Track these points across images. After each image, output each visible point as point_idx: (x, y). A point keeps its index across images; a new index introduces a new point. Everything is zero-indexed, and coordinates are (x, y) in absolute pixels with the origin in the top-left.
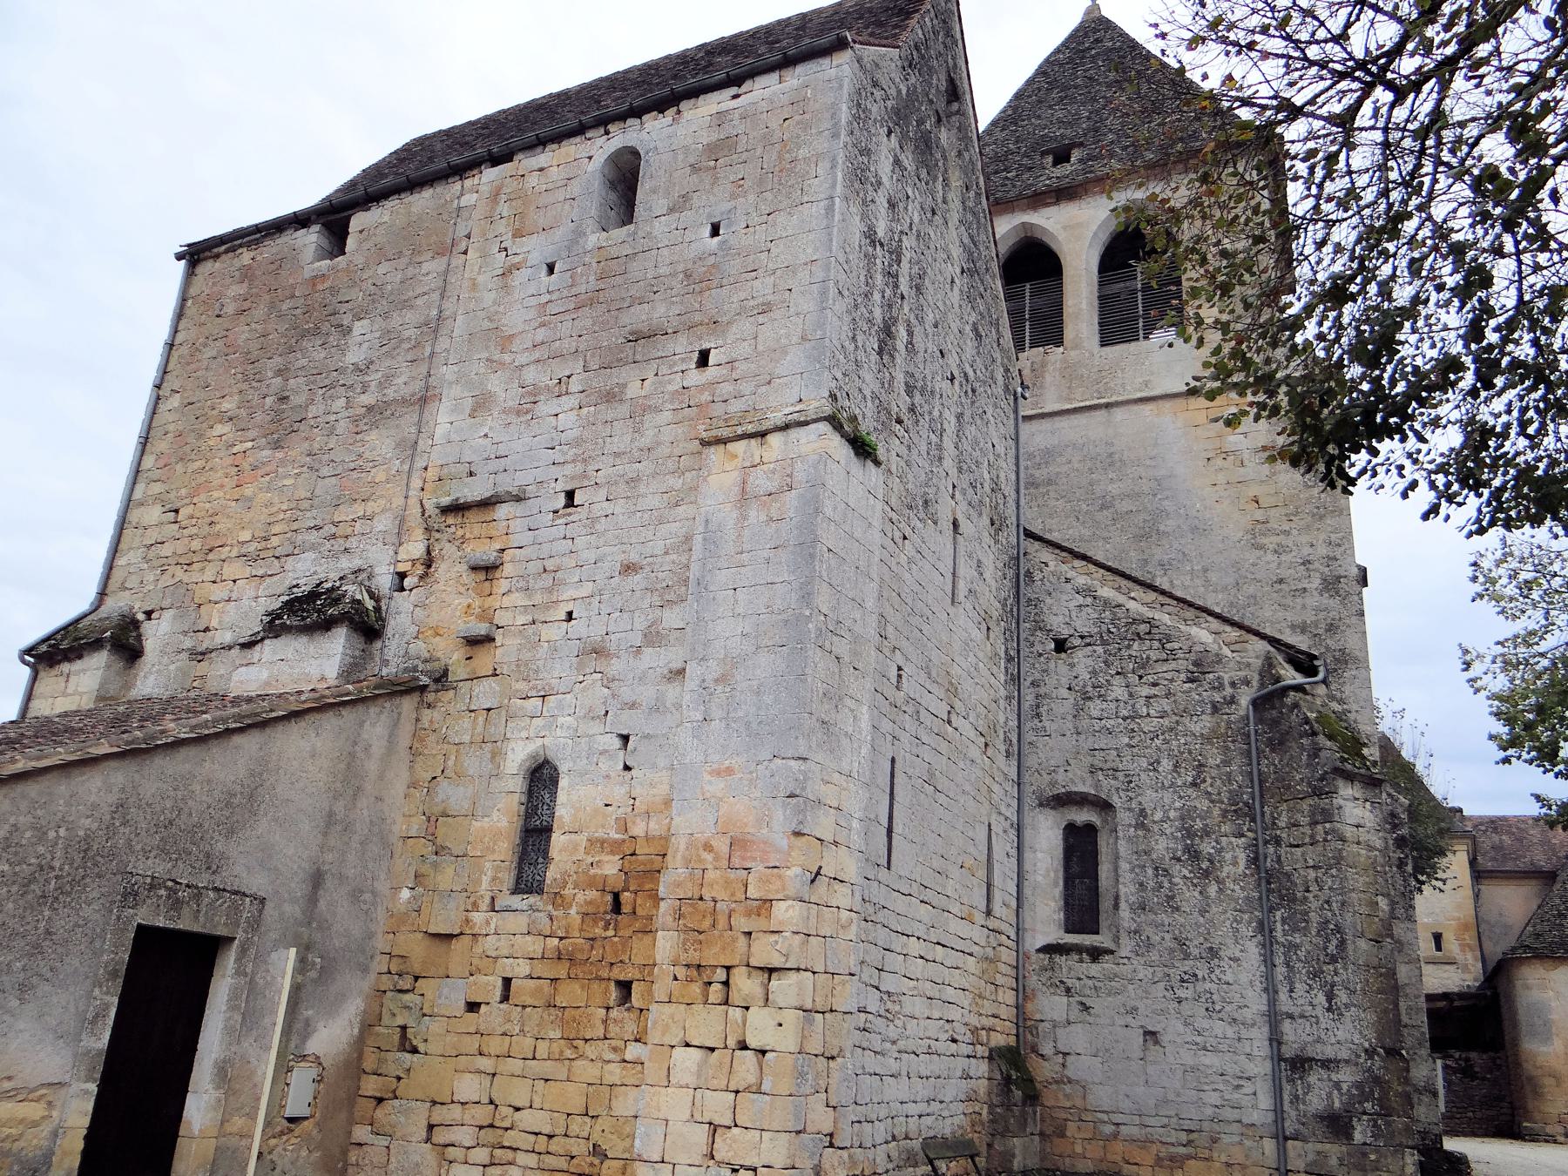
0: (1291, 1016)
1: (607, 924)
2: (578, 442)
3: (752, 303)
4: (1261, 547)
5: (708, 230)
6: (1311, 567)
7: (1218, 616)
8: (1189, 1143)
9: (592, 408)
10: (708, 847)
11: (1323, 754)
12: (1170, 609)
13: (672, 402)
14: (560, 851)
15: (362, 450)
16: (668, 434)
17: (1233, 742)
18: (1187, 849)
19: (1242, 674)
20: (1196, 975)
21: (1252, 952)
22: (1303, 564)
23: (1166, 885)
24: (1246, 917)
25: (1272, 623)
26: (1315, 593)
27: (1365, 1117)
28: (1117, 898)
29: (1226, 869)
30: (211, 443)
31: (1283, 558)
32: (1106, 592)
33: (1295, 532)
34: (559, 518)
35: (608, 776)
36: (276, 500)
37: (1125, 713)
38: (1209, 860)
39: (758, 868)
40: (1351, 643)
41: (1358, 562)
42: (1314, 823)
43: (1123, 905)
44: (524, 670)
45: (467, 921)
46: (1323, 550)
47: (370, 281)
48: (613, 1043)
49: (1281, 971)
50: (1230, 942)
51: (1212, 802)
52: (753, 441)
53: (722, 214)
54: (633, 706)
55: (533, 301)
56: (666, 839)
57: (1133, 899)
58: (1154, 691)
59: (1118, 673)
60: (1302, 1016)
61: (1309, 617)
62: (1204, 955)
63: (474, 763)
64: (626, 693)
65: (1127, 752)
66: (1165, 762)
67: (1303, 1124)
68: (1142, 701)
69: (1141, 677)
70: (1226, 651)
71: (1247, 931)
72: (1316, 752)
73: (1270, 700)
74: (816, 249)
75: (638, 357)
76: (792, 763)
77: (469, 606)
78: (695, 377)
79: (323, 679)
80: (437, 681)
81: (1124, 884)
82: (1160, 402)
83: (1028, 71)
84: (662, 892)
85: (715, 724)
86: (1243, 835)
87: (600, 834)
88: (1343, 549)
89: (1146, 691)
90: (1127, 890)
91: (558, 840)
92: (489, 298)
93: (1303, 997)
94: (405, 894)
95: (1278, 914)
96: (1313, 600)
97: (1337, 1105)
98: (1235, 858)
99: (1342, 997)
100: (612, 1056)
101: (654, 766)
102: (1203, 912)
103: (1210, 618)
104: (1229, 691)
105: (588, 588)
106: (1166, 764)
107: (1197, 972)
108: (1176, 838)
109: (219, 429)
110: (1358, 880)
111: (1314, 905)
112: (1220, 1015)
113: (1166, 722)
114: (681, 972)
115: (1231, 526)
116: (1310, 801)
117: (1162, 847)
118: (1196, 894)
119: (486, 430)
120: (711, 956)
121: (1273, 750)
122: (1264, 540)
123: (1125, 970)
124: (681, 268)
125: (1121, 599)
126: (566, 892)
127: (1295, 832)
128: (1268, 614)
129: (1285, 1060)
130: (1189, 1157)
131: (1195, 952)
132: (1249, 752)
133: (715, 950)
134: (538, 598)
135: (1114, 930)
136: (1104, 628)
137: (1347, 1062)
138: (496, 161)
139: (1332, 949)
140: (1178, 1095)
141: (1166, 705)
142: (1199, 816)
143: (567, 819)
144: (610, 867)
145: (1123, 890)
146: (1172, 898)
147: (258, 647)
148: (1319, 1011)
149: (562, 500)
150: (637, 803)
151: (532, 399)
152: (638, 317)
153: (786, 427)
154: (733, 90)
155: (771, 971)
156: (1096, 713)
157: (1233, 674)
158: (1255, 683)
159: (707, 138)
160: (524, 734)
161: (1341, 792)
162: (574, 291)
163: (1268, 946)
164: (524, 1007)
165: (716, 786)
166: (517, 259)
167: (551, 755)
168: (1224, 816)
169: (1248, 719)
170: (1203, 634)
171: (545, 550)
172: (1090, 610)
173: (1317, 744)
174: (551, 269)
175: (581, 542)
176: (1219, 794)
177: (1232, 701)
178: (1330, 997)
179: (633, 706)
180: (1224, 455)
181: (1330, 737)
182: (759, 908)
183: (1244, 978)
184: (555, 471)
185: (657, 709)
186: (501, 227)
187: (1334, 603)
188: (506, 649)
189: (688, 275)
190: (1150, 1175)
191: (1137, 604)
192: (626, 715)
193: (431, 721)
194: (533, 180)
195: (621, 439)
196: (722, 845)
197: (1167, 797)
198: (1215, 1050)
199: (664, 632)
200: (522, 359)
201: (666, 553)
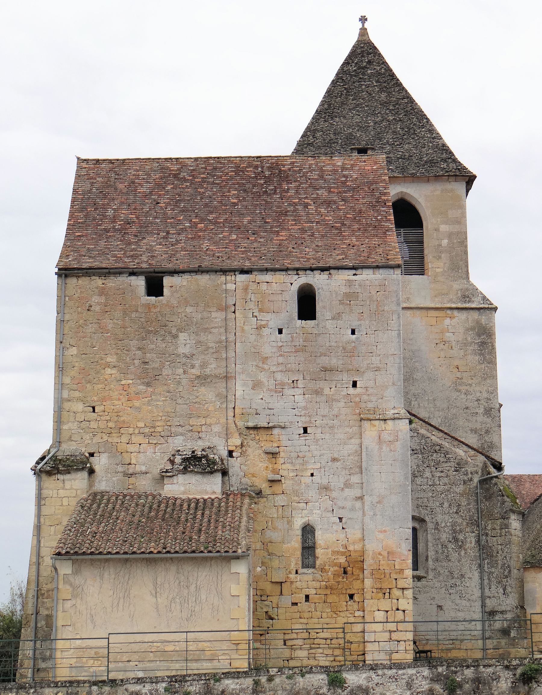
0: (490, 597)
1: (343, 578)
2: (305, 408)
3: (372, 366)
4: (459, 391)
6: (480, 402)
7: (467, 445)
8: (453, 643)
9: (310, 396)
10: (380, 554)
11: (506, 504)
12: (448, 440)
13: (344, 399)
14: (322, 555)
15: (198, 394)
16: (344, 411)
17: (471, 496)
18: (454, 538)
19: (475, 469)
20: (456, 585)
21: (476, 575)
22: (477, 401)
23: (446, 551)
24: (474, 562)
25: (463, 428)
26: (481, 415)
27: (515, 628)
28: (427, 557)
29: (468, 545)
30: (106, 377)
31: (469, 397)
32: (423, 431)
33: (474, 385)
34: (302, 437)
35: (337, 531)
36: (155, 410)
37: (430, 483)
38: (462, 542)
39: (398, 560)
40: (495, 439)
42: (501, 529)
43: (430, 559)
44: (296, 493)
45: (288, 577)
46: (485, 395)
47: (183, 315)
48: (350, 612)
49: (486, 582)
50: (468, 572)
51: (463, 519)
52: (381, 421)
53: (356, 326)
54: (343, 508)
55: (274, 344)
56: (363, 552)
57: (433, 557)
58: (442, 474)
59: (427, 466)
60: (494, 597)
61: (478, 426)
62: (459, 577)
63: (280, 525)
64: (340, 504)
65: (431, 499)
66: (446, 504)
67: (493, 633)
68: (437, 478)
69: (436, 468)
70: (469, 459)
71: (474, 567)
72: (503, 502)
73: (486, 481)
74: (395, 350)
75: (327, 378)
76: (406, 529)
77: (267, 467)
78: (352, 391)
79: (214, 493)
80: (257, 494)
81: (430, 551)
82: (415, 310)
83: (331, 76)
84: (365, 567)
85: (378, 516)
86: (474, 532)
87: (336, 549)
88: (493, 395)
89: (439, 474)
90: (431, 554)
91: (319, 552)
92: (253, 338)
93: (495, 590)
94: (259, 569)
95: (486, 561)
96: (480, 418)
97: (505, 625)
98: (471, 540)
99: (509, 589)
100: (350, 615)
101: (354, 528)
102: (459, 561)
103: (464, 446)
104: (470, 476)
106: (446, 505)
107: (457, 583)
108: (450, 533)
109: (109, 371)
110: (515, 548)
111: (500, 558)
112: (464, 598)
113: (446, 487)
114: (375, 590)
115: (446, 379)
116: (500, 520)
117: (444, 537)
118: (457, 555)
119: (261, 397)
120: (385, 585)
121: (486, 500)
122: (460, 388)
123: (431, 584)
124: (341, 345)
125: (429, 435)
126: (326, 568)
127: (494, 531)
128: (461, 423)
129: (487, 612)
130: (453, 649)
131: (456, 576)
132: (477, 500)
133: (386, 584)
134: (297, 467)
135: (426, 569)
136: (422, 447)
137: (510, 611)
138: (243, 272)
139: (506, 573)
140: (449, 627)
141: (446, 480)
142: (458, 525)
143: (322, 544)
144: (342, 560)
145: (430, 554)
146: (448, 556)
147: (175, 477)
148: (500, 595)
149: (302, 431)
150: (349, 540)
151: (282, 387)
152: (324, 361)
153: (394, 419)
154: (354, 272)
155: (403, 589)
156: (419, 483)
157: (471, 469)
158: (480, 473)
159: (344, 290)
160: (300, 516)
161: (511, 518)
162: (293, 344)
163: (481, 573)
164: (315, 603)
165: (381, 536)
166: (263, 323)
167: (311, 523)
168: (467, 525)
169: (477, 487)
170: (461, 452)
171: (298, 449)
172: (416, 438)
173: (504, 499)
174: (280, 331)
175: (313, 447)
176: (466, 516)
177: (471, 480)
178: (504, 590)
179: (343, 508)
180: (444, 343)
181: (508, 497)
182: (399, 572)
183: (473, 585)
184: (298, 419)
185: (353, 509)
186: (251, 305)
187: (489, 420)
188: (287, 484)
189: (344, 349)
191: (435, 438)
192: (341, 510)
193: (258, 509)
194: (264, 286)
195: (324, 410)
196: (385, 554)
197: (447, 517)
198: (462, 611)
199: (352, 484)
200: (274, 369)
201: (349, 456)
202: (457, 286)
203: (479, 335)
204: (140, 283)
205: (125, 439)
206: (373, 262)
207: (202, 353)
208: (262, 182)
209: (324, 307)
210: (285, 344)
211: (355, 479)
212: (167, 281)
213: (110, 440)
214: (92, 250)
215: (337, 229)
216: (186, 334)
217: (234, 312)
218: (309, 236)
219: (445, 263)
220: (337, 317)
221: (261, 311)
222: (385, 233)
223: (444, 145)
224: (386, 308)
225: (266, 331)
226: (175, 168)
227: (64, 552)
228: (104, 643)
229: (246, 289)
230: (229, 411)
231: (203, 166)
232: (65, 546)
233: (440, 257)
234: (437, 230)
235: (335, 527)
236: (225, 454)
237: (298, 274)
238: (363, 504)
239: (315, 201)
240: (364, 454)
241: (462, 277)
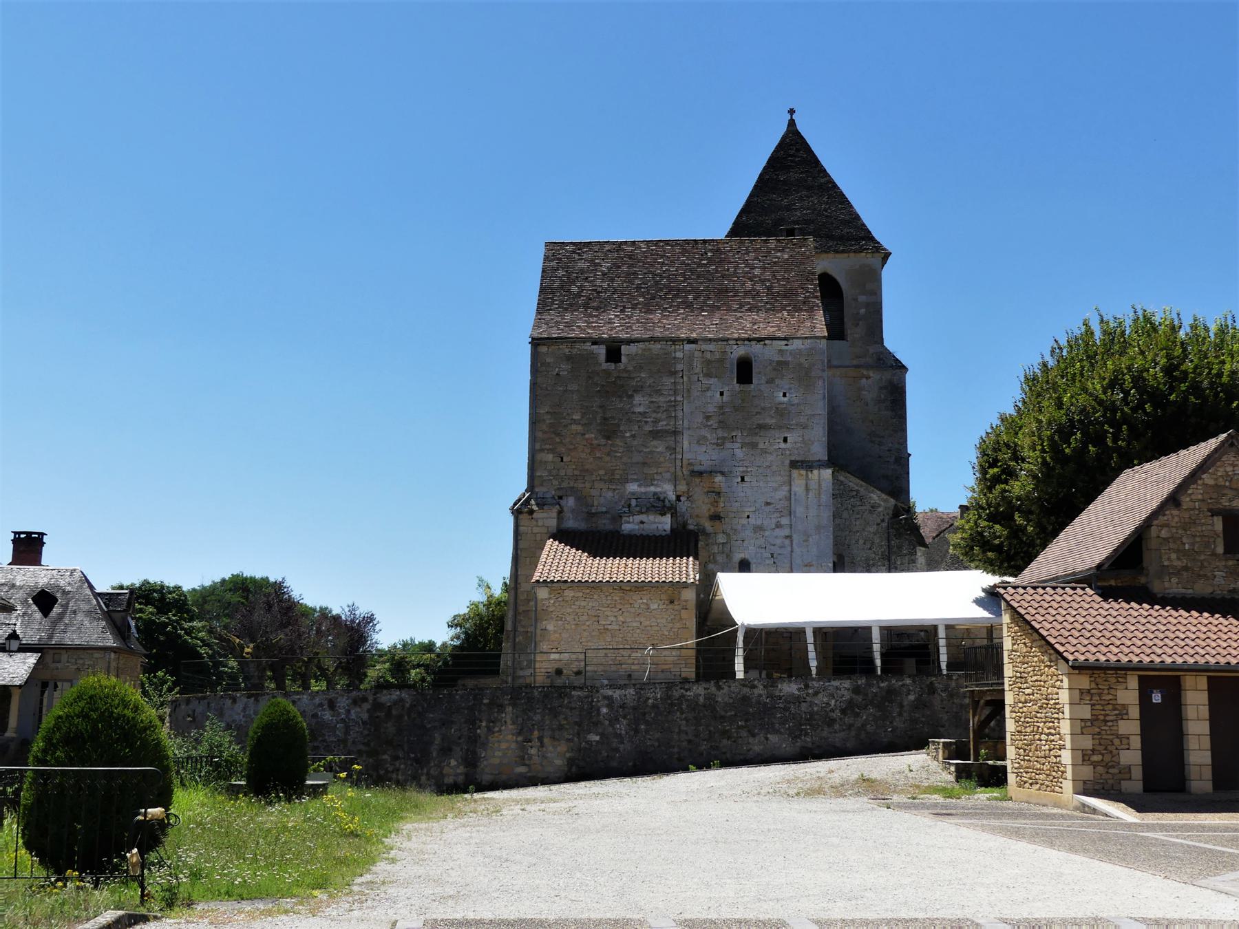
5: (782, 394)
41: (717, 225)
78: (783, 445)
105: (754, 509)
106: (861, 542)
149: (740, 479)
154: (785, 342)
179: (774, 545)
185: (782, 547)
190: (4, 874)
202: (872, 350)
204: (601, 350)
205: (588, 485)
206: (802, 334)
211: (785, 521)
213: (575, 485)
214: (559, 322)
215: (771, 304)
217: (682, 377)
220: (770, 381)
227: (541, 580)
228: (582, 657)
230: (677, 461)
233: (858, 324)
234: (856, 300)
235: (767, 562)
236: (674, 498)
237: (737, 344)
238: (792, 541)
240: (792, 499)
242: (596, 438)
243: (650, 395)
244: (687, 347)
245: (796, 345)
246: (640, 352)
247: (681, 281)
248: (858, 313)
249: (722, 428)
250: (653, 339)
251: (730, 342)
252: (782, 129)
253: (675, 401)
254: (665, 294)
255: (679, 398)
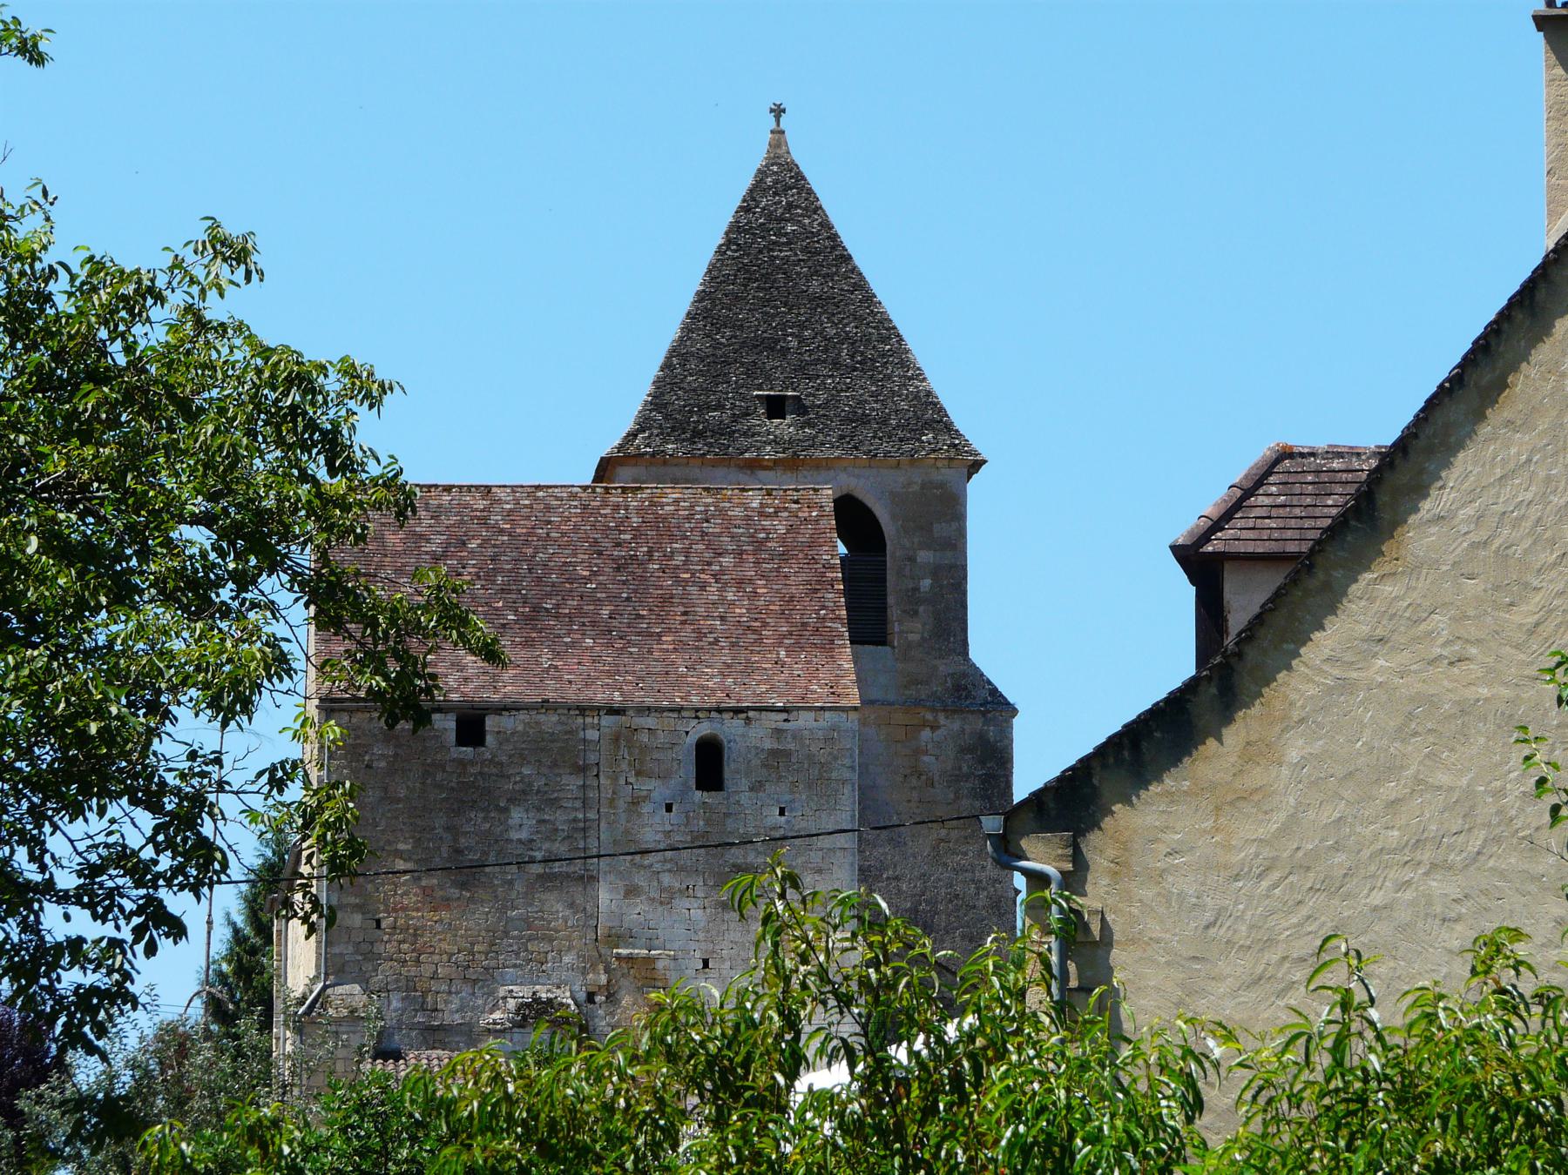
154: (784, 716)
174: (669, 808)
200: (657, 867)
202: (944, 667)
203: (982, 762)
207: (548, 839)
208: (628, 537)
209: (737, 772)
210: (676, 828)
212: (491, 722)
215: (755, 631)
216: (521, 809)
218: (710, 644)
219: (924, 625)
220: (756, 787)
221: (638, 774)
222: (832, 642)
223: (929, 393)
224: (834, 775)
225: (646, 808)
226: (481, 504)
229: (616, 740)
231: (527, 502)
232: (607, 1132)
233: (916, 613)
234: (912, 559)
237: (697, 717)
239: (716, 577)
241: (954, 651)
242: (441, 887)
243: (539, 809)
244: (607, 721)
245: (804, 720)
246: (520, 728)
247: (584, 577)
248: (916, 589)
249: (670, 871)
250: (546, 706)
251: (684, 714)
252: (756, 157)
253: (585, 820)
254: (557, 606)
255: (592, 815)
